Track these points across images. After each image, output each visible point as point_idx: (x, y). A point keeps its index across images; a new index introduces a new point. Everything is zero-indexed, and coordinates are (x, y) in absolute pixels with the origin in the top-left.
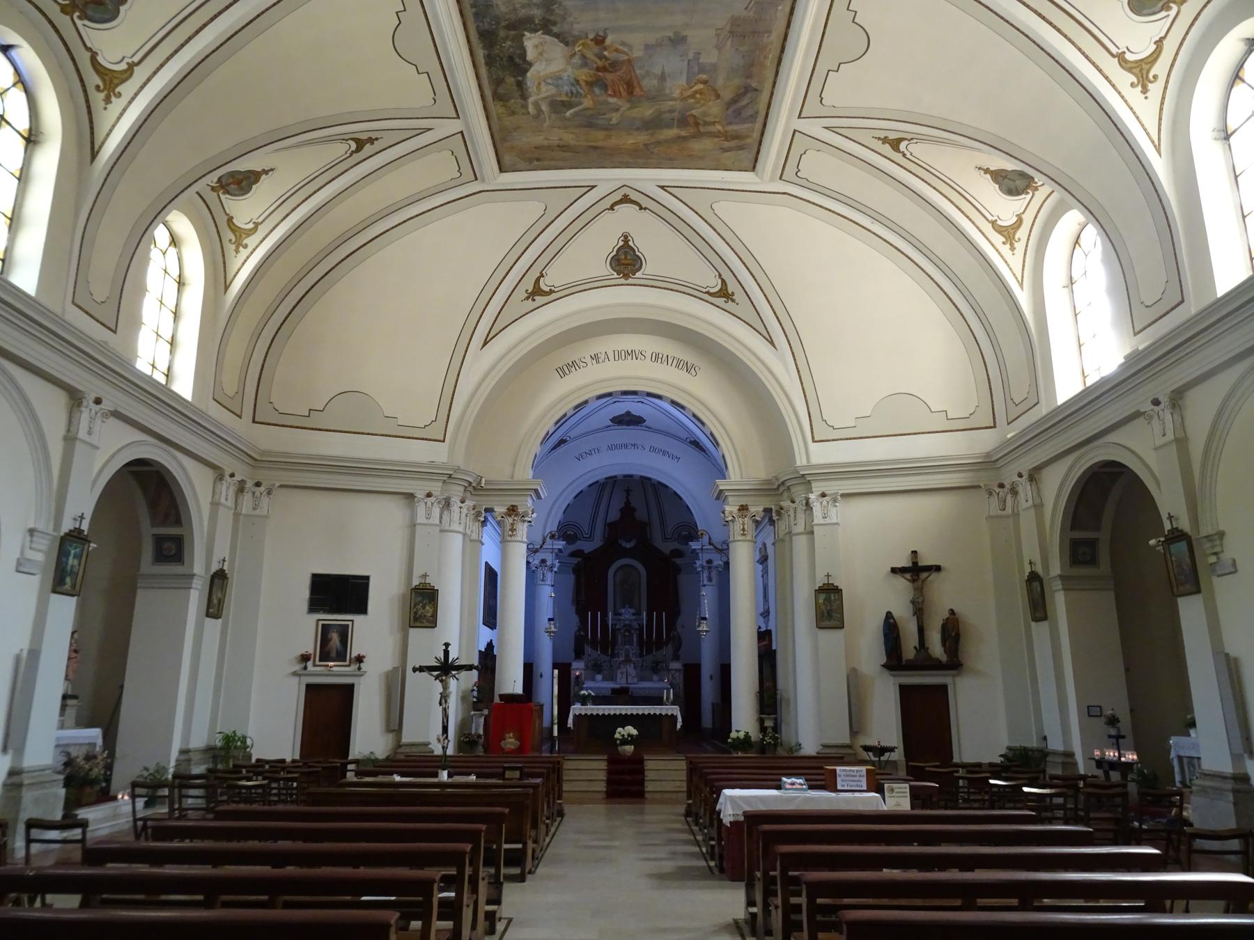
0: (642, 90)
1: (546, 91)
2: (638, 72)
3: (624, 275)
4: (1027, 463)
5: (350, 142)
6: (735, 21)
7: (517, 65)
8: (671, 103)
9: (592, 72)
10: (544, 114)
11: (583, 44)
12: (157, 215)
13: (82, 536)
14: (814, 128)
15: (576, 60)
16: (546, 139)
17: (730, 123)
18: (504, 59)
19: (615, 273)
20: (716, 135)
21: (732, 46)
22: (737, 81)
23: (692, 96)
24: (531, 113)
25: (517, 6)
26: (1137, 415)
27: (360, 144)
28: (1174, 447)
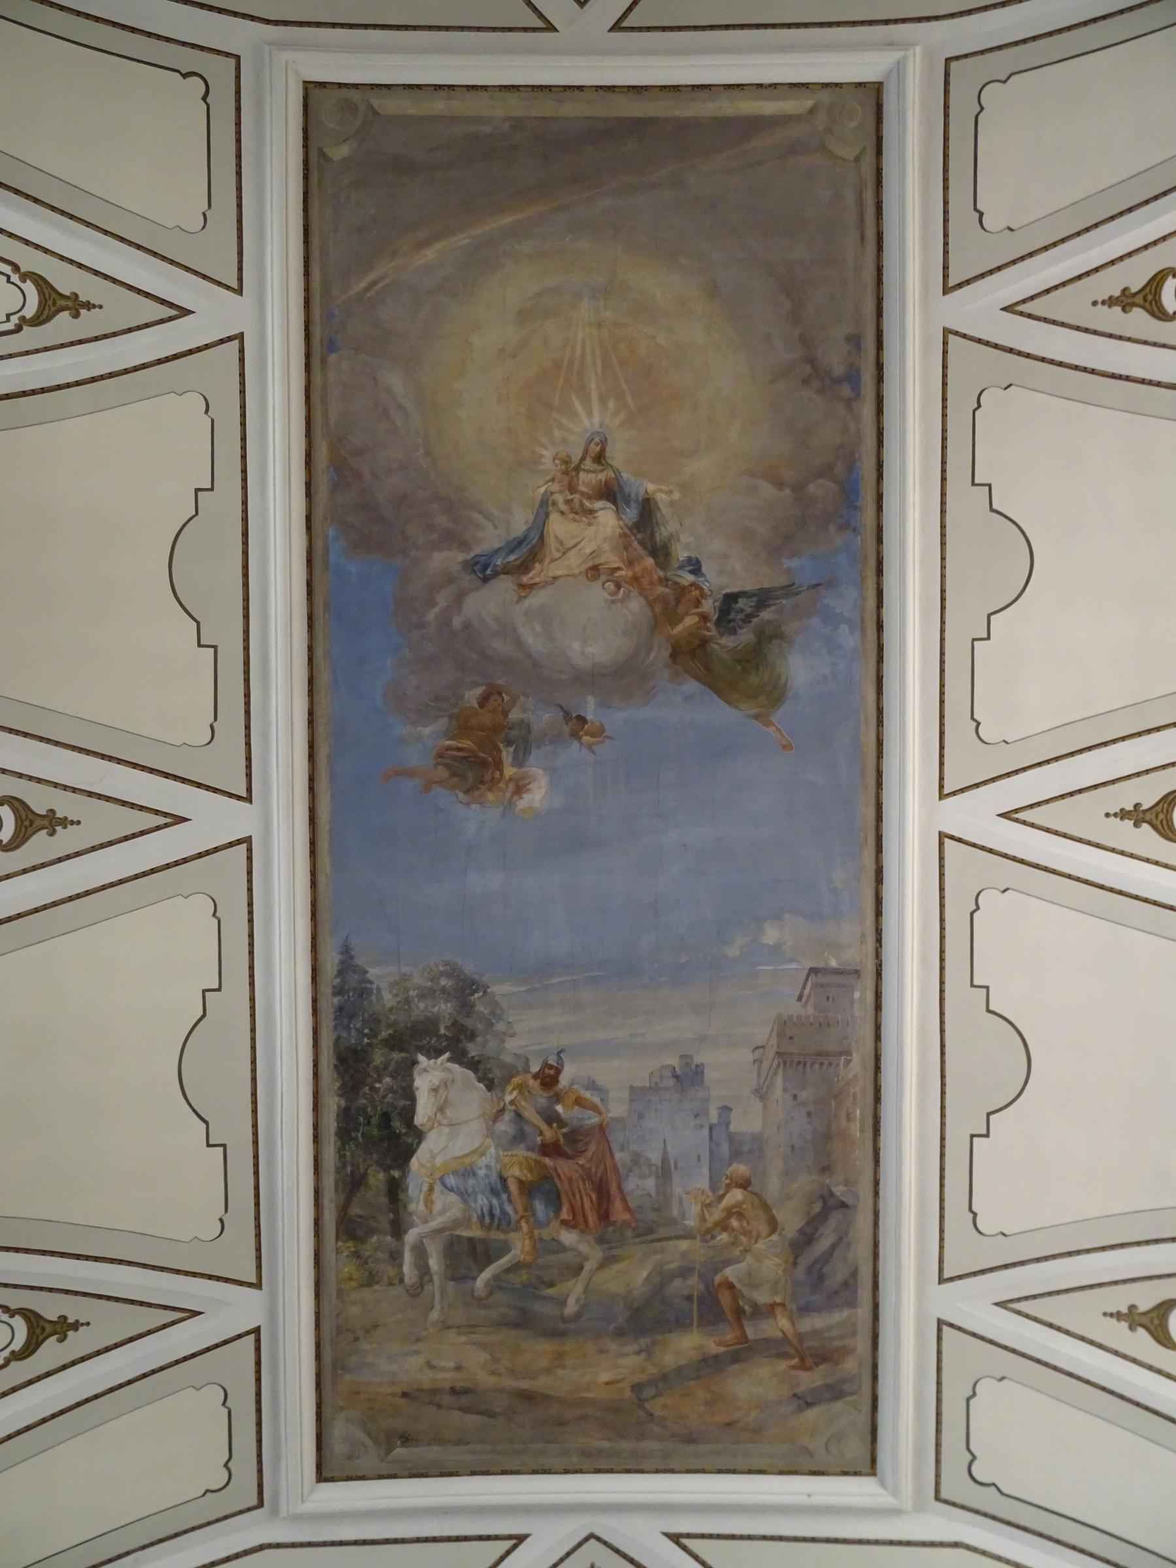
0: (627, 1208)
1: (444, 1211)
2: (618, 1155)
6: (784, 1028)
7: (396, 1137)
8: (684, 1245)
9: (533, 1155)
10: (431, 1280)
11: (521, 1087)
15: (505, 1126)
16: (430, 1366)
17: (805, 1310)
18: (374, 1121)
20: (777, 1348)
21: (785, 1090)
22: (805, 1182)
23: (723, 1225)
24: (407, 1279)
25: (412, 993)
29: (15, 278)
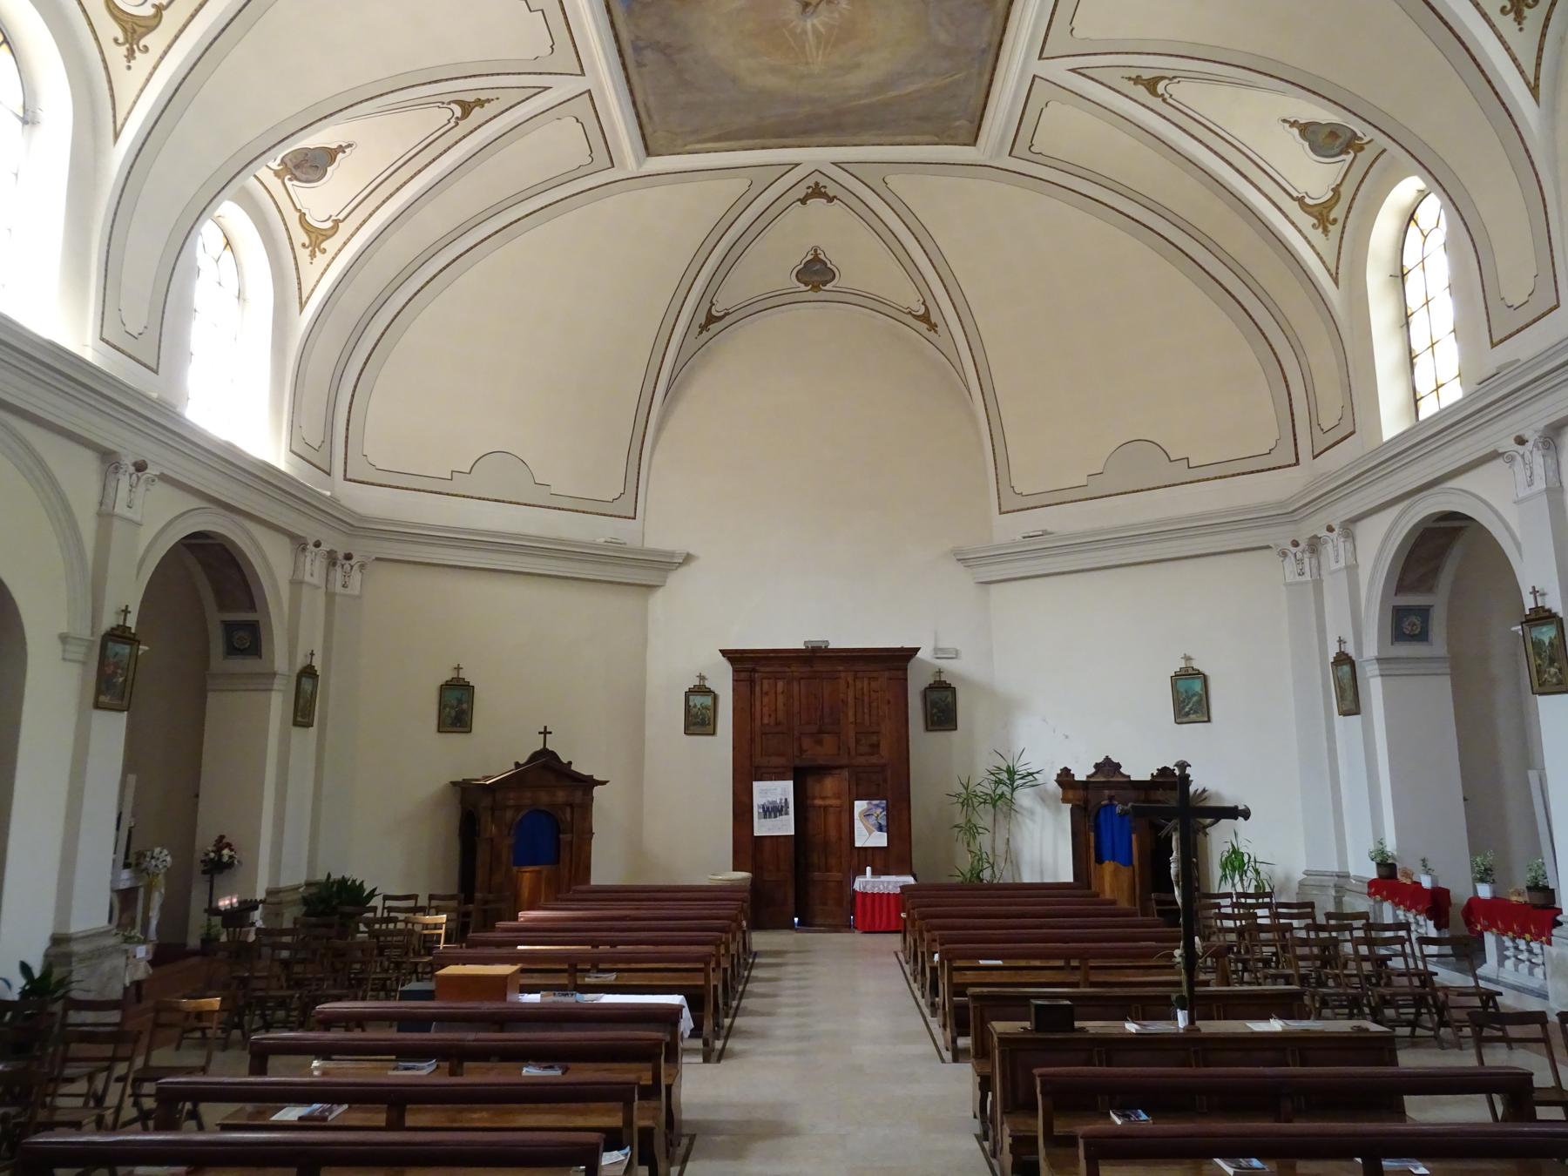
3: (813, 287)
4: (1340, 512)
5: (453, 106)
12: (202, 210)
13: (127, 635)
14: (1057, 70)
19: (802, 285)
26: (1494, 455)
27: (467, 108)
28: (1544, 499)
29: (1167, 96)
